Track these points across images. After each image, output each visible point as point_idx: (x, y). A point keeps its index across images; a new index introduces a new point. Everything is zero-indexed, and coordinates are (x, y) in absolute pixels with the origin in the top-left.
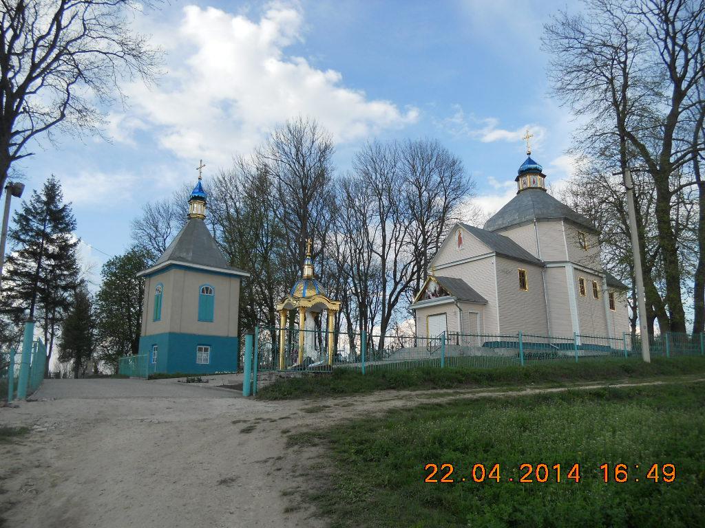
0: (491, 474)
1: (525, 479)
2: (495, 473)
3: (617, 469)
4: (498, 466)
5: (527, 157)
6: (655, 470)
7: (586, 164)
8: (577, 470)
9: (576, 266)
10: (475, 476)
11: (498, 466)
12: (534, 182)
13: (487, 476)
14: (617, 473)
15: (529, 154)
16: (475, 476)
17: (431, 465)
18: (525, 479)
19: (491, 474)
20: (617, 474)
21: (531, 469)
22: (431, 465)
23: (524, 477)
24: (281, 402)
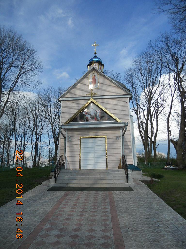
0: (19, 174)
1: (17, 185)
2: (19, 175)
3: (21, 218)
4: (22, 176)
5: (94, 55)
6: (20, 203)
7: (133, 67)
8: (20, 204)
9: (114, 114)
10: (18, 190)
11: (22, 176)
12: (15, 64)
13: (19, 172)
14: (19, 235)
15: (95, 54)
16: (18, 190)
17: (22, 186)
18: (17, 185)
19: (19, 174)
20: (19, 218)
21: (21, 188)
22: (22, 186)
23: (18, 185)
24: (135, 171)
